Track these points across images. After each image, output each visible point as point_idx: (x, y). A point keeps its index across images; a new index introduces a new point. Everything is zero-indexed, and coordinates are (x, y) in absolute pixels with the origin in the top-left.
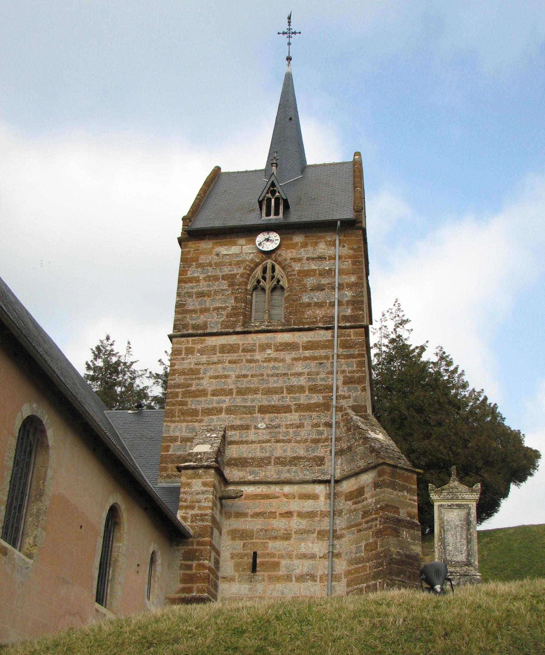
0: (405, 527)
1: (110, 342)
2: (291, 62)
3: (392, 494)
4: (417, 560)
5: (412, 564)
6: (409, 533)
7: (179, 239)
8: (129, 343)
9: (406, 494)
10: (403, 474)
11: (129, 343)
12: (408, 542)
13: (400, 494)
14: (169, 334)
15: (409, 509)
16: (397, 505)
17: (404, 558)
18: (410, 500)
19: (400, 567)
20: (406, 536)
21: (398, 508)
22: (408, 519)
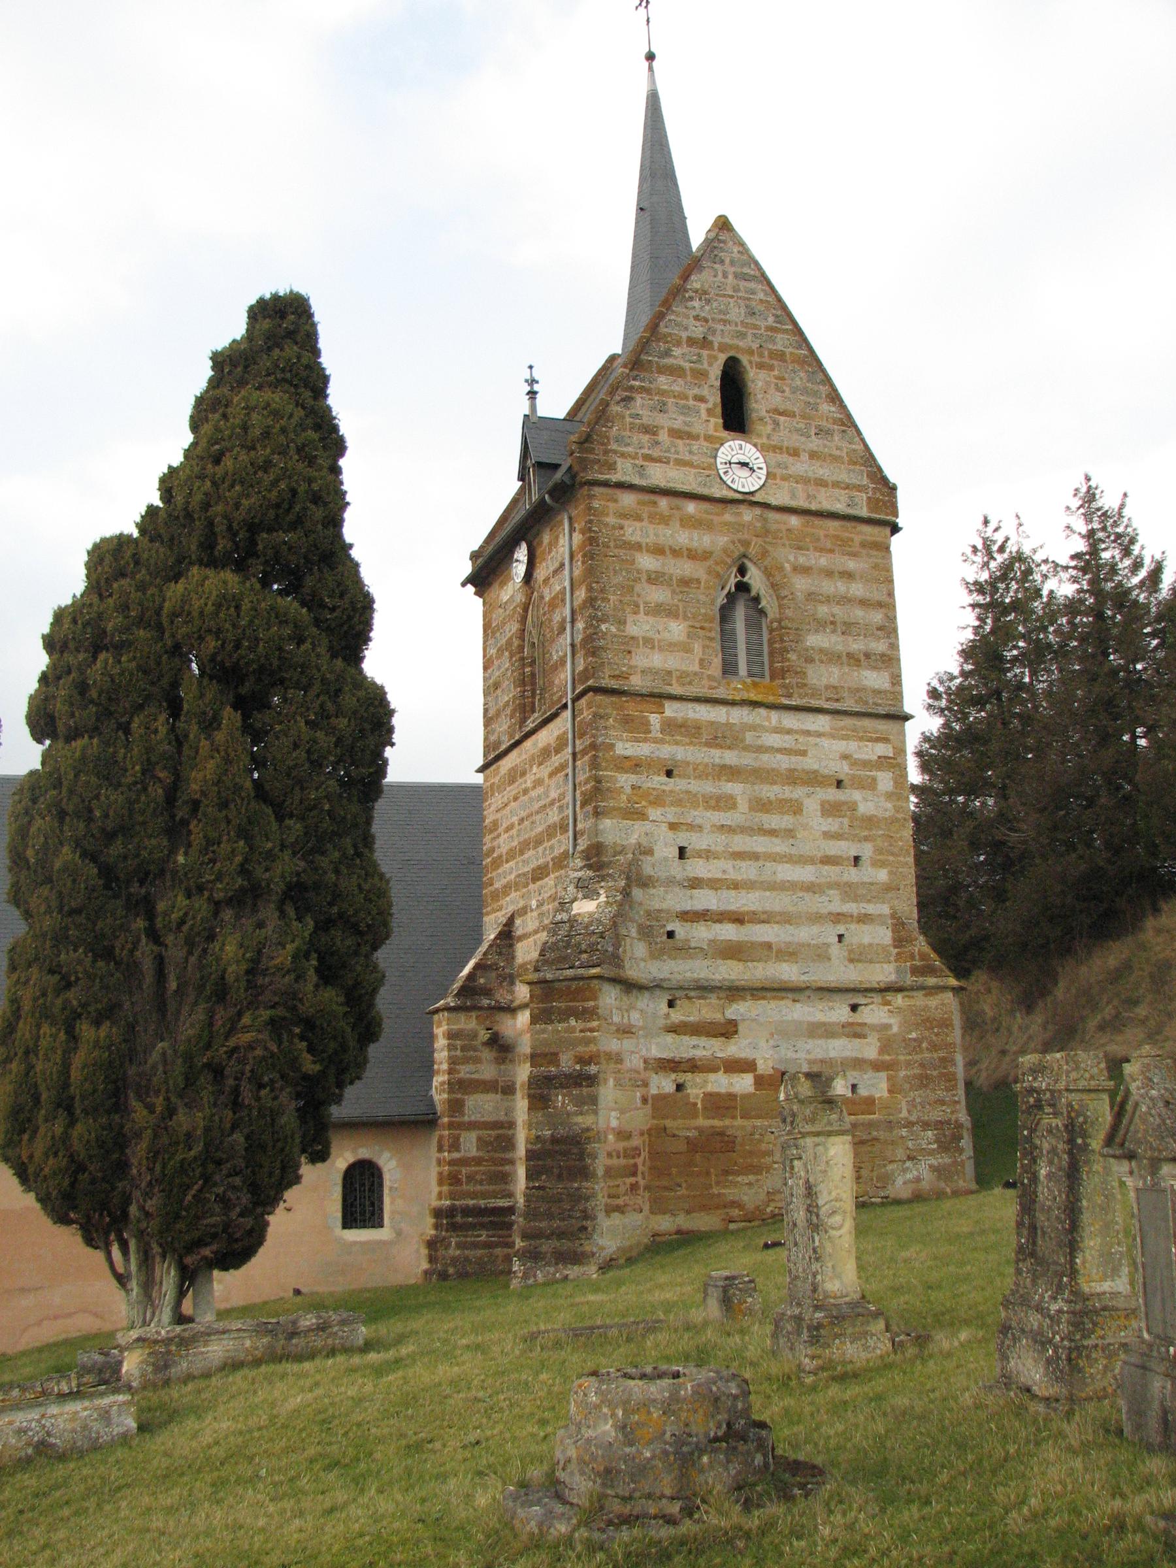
0: (562, 1086)
1: (992, 526)
2: (654, 63)
3: (544, 1031)
4: (578, 1143)
5: (565, 1154)
6: (570, 1095)
7: (44, 637)
8: (1125, 495)
9: (573, 1022)
10: (568, 988)
11: (1125, 495)
12: (568, 1114)
13: (560, 1027)
14: (396, 715)
15: (580, 1049)
16: (554, 1049)
17: (548, 1146)
18: (581, 1031)
19: (540, 1163)
20: (563, 1103)
21: (556, 1054)
22: (578, 1067)
